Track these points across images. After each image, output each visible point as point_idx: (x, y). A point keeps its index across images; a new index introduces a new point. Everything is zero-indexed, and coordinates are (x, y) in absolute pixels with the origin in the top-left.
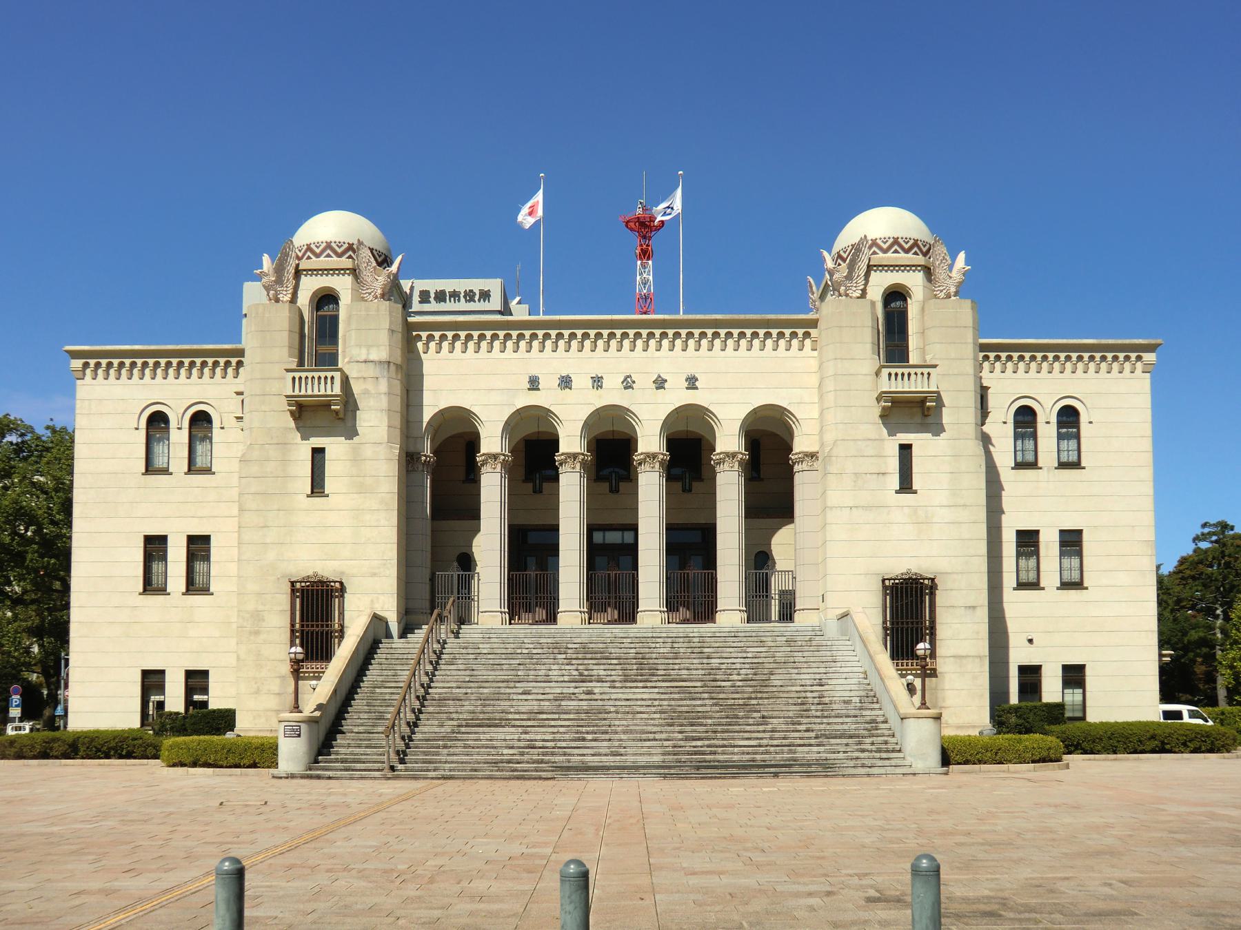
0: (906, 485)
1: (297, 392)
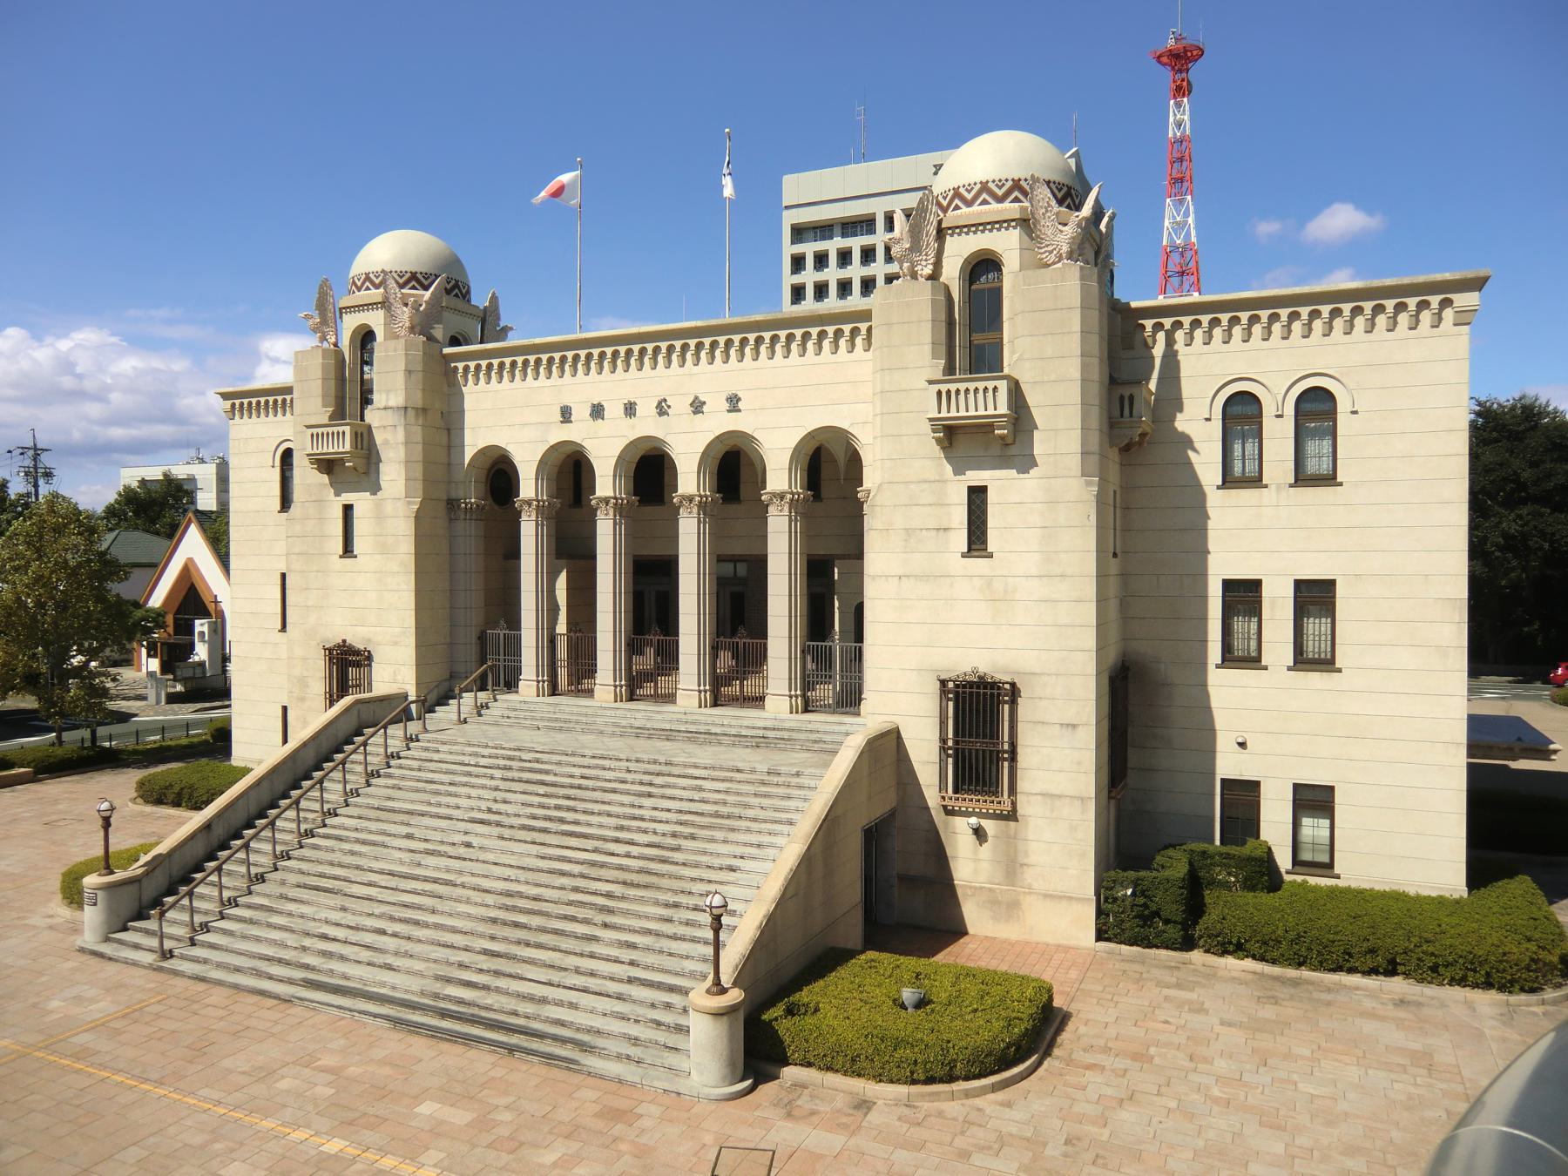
0: (977, 539)
1: (944, 414)
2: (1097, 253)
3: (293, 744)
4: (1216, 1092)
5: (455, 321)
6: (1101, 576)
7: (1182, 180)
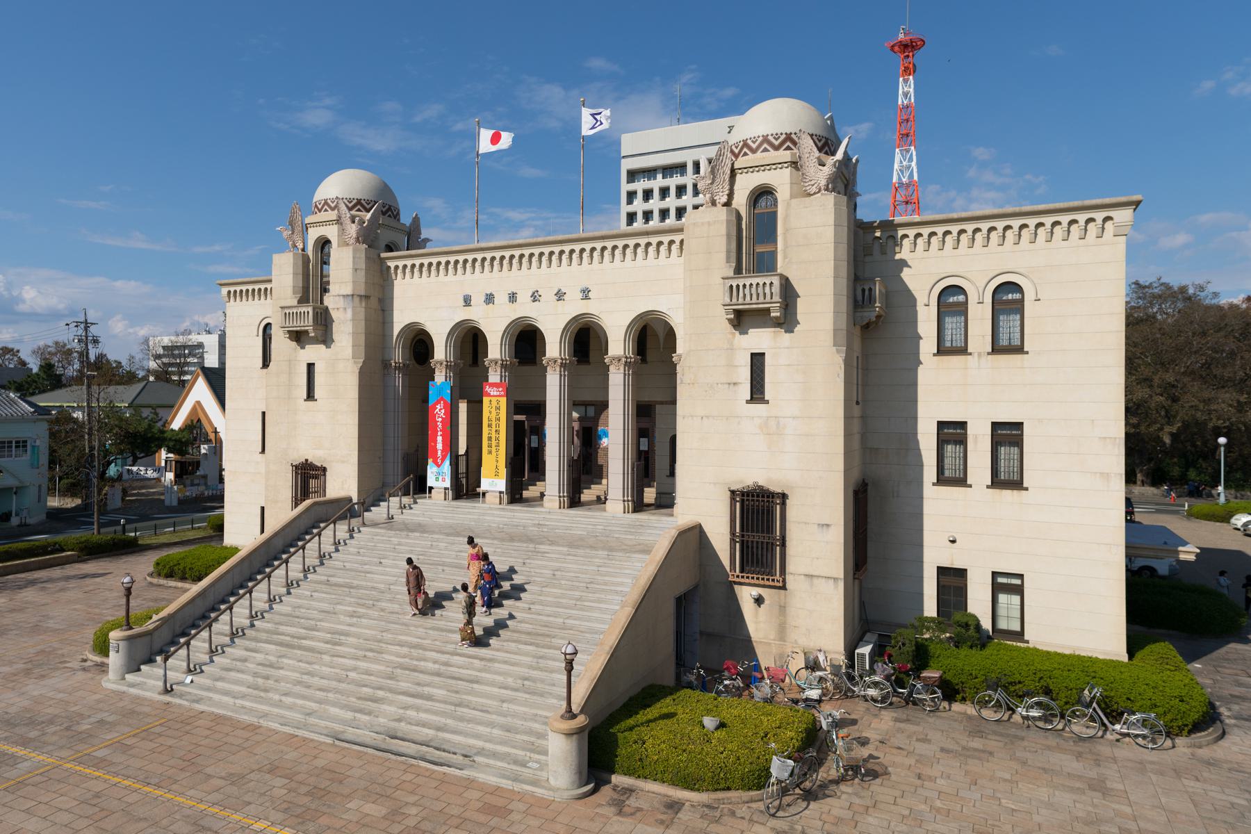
0: (757, 392)
2: (846, 186)
3: (269, 530)
4: (938, 804)
5: (389, 232)
6: (848, 418)
7: (907, 135)
